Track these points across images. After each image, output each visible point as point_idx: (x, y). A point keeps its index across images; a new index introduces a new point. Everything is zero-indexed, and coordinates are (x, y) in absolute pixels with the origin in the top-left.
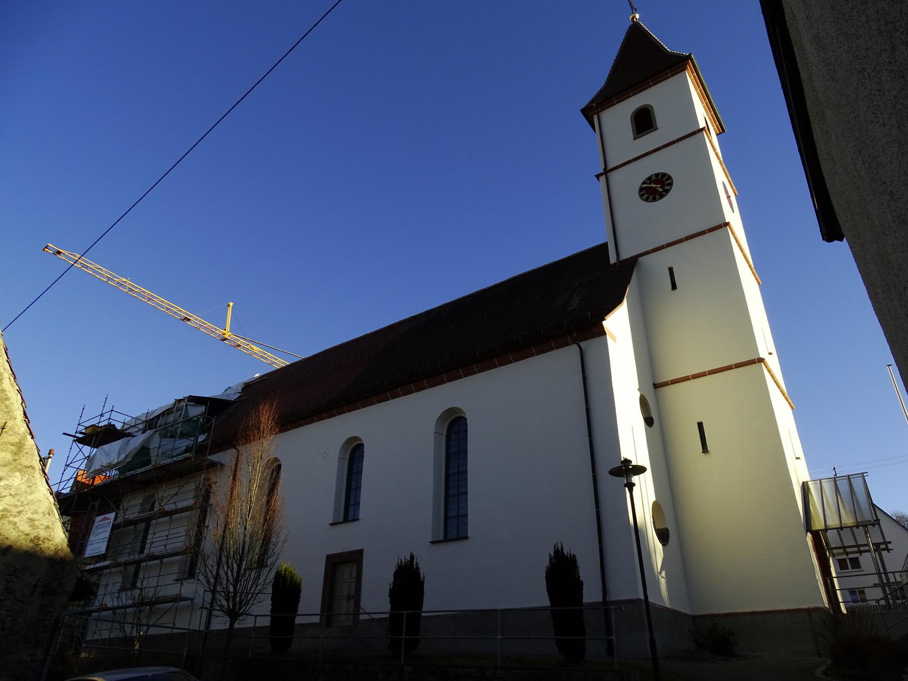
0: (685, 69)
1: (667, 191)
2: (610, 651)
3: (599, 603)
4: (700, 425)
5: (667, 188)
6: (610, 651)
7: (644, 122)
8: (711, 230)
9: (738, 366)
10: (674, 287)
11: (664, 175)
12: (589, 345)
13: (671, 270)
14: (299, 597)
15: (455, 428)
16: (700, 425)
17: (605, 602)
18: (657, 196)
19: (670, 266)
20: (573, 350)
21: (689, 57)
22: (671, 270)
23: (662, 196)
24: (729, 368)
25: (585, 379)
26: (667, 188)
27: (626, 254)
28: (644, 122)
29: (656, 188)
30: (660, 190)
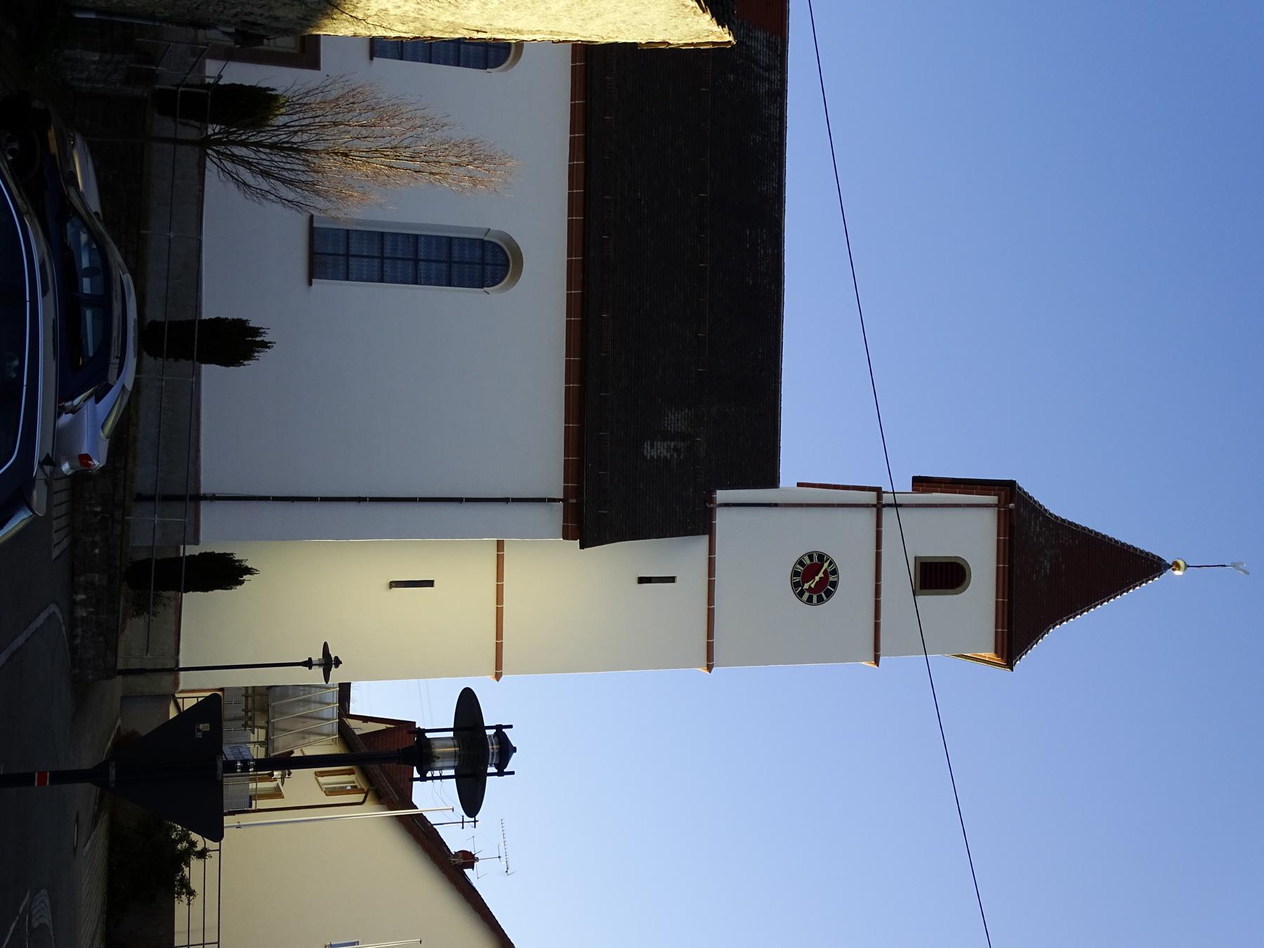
0: (996, 652)
1: (800, 595)
2: (141, 498)
3: (200, 314)
4: (430, 583)
5: (806, 595)
6: (141, 498)
7: (941, 576)
8: (710, 647)
9: (499, 647)
10: (642, 580)
11: (829, 594)
12: (556, 514)
13: (672, 580)
14: (212, 590)
15: (481, 262)
16: (430, 583)
17: (198, 498)
18: (798, 579)
19: (677, 580)
20: (556, 488)
21: (1010, 665)
22: (672, 580)
23: (795, 585)
24: (499, 635)
25: (506, 500)
26: (806, 595)
27: (723, 519)
28: (941, 576)
29: (814, 579)
30: (806, 586)
